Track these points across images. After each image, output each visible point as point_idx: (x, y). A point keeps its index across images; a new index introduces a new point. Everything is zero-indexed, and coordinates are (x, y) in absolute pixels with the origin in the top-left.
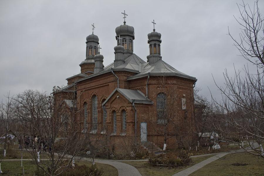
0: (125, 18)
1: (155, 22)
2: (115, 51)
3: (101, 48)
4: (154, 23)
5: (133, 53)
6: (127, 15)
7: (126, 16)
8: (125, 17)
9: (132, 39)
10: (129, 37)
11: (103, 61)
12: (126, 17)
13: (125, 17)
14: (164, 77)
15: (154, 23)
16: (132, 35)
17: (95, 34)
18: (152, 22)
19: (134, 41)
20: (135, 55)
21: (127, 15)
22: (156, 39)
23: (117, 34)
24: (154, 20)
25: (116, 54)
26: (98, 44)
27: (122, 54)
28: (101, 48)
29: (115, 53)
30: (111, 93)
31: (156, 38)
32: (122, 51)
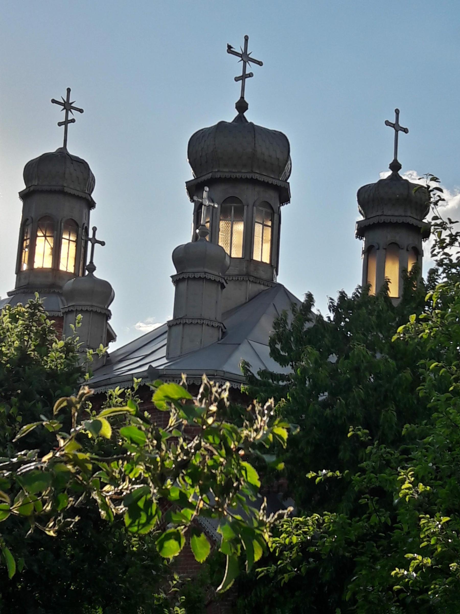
0: (64, 120)
1: (401, 124)
2: (175, 272)
3: (103, 244)
4: (396, 127)
5: (279, 279)
6: (260, 64)
7: (251, 68)
8: (244, 77)
9: (274, 201)
10: (257, 189)
11: (108, 315)
12: (251, 75)
13: (244, 77)
14: (373, 328)
15: (396, 127)
16: (275, 182)
17: (72, 151)
18: (387, 123)
19: (284, 209)
20: (284, 288)
21: (260, 64)
22: (400, 220)
23: (244, 117)
24: (397, 112)
25: (183, 286)
26: (91, 205)
27: (211, 289)
28: (103, 244)
29: (176, 280)
30: (234, 210)
31: (400, 212)
32: (214, 273)
